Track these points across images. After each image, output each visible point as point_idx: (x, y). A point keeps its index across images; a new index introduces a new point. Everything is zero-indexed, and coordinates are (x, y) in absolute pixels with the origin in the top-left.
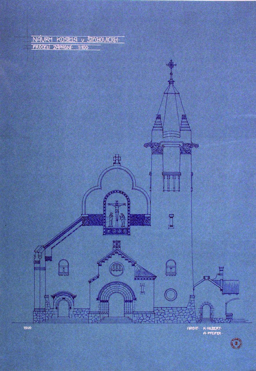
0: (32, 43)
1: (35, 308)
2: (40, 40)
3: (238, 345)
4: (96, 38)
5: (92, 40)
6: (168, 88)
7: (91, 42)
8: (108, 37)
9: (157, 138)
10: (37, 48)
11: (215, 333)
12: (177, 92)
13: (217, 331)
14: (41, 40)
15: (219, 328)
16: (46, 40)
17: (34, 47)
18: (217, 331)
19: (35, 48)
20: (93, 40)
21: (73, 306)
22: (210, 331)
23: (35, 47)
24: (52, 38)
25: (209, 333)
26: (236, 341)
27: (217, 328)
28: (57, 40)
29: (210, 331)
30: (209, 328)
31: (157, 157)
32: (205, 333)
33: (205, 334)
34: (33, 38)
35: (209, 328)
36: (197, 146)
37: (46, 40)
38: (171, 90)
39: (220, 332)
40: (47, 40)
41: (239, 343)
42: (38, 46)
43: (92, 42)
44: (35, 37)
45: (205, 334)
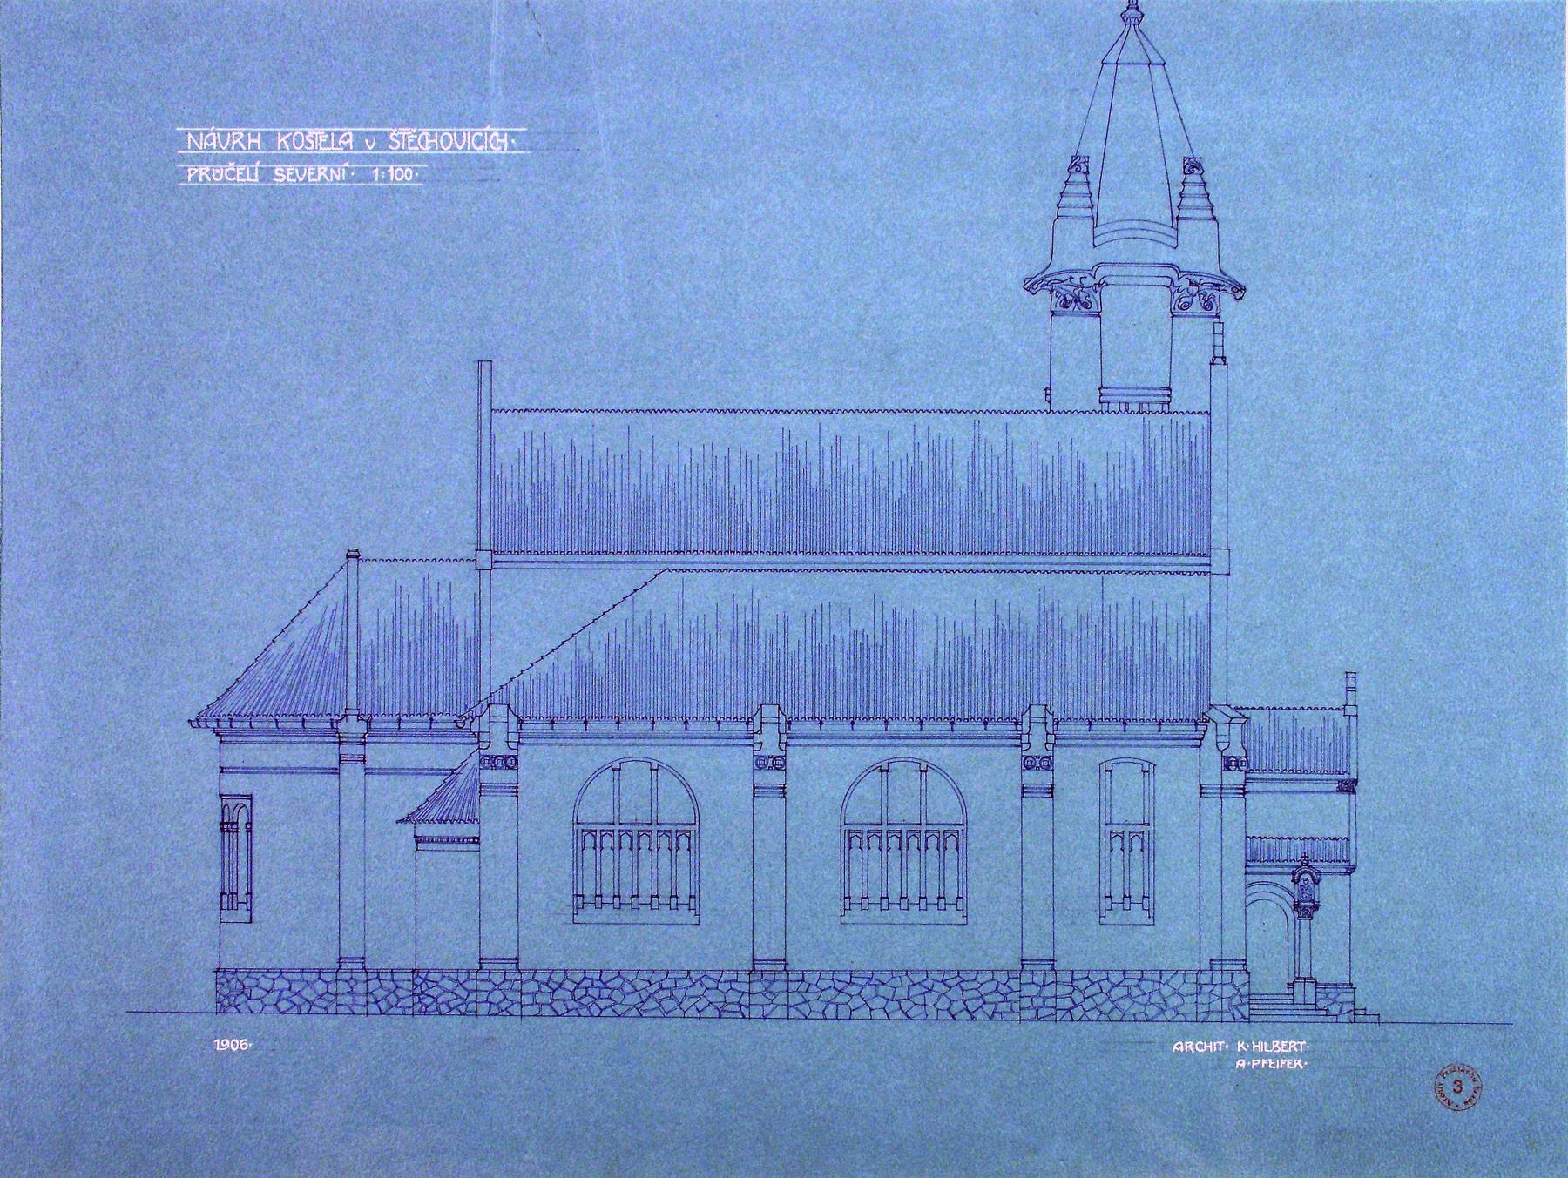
0: (182, 158)
1: (483, 955)
2: (214, 143)
3: (1465, 1095)
4: (421, 136)
5: (406, 142)
6: (1122, 40)
7: (400, 149)
8: (472, 134)
9: (1075, 252)
10: (204, 177)
11: (1283, 1062)
12: (1159, 60)
13: (1292, 1055)
14: (217, 143)
15: (1298, 1046)
16: (234, 142)
17: (190, 176)
18: (1292, 1055)
19: (195, 179)
20: (409, 141)
21: (878, 851)
22: (1263, 1055)
23: (198, 173)
24: (259, 135)
25: (1254, 1063)
26: (1461, 1076)
27: (1293, 1044)
28: (280, 141)
29: (1263, 1055)
30: (1260, 1046)
31: (1075, 326)
32: (1241, 1063)
33: (1243, 1065)
34: (190, 136)
35: (1260, 1046)
36: (1239, 289)
37: (234, 142)
38: (1133, 52)
39: (1300, 1061)
40: (237, 145)
41: (1468, 1086)
42: (242, 135)
43: (406, 149)
44: (196, 134)
45: (1243, 1065)
